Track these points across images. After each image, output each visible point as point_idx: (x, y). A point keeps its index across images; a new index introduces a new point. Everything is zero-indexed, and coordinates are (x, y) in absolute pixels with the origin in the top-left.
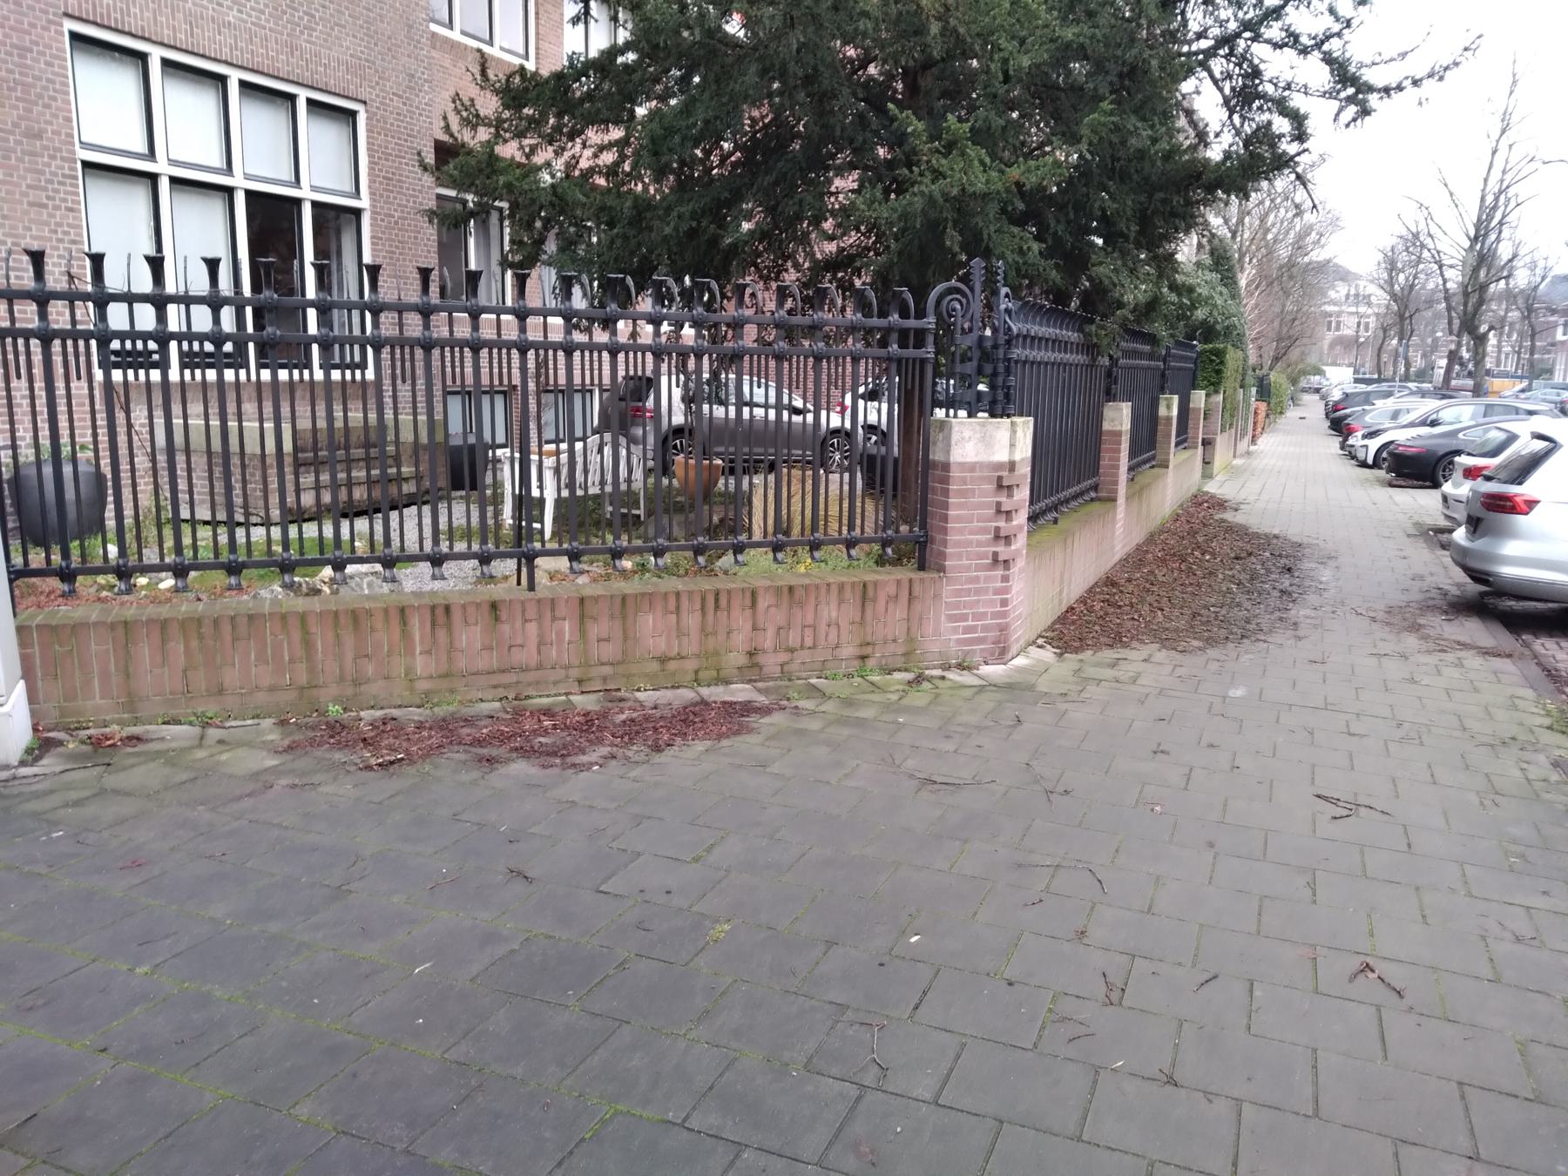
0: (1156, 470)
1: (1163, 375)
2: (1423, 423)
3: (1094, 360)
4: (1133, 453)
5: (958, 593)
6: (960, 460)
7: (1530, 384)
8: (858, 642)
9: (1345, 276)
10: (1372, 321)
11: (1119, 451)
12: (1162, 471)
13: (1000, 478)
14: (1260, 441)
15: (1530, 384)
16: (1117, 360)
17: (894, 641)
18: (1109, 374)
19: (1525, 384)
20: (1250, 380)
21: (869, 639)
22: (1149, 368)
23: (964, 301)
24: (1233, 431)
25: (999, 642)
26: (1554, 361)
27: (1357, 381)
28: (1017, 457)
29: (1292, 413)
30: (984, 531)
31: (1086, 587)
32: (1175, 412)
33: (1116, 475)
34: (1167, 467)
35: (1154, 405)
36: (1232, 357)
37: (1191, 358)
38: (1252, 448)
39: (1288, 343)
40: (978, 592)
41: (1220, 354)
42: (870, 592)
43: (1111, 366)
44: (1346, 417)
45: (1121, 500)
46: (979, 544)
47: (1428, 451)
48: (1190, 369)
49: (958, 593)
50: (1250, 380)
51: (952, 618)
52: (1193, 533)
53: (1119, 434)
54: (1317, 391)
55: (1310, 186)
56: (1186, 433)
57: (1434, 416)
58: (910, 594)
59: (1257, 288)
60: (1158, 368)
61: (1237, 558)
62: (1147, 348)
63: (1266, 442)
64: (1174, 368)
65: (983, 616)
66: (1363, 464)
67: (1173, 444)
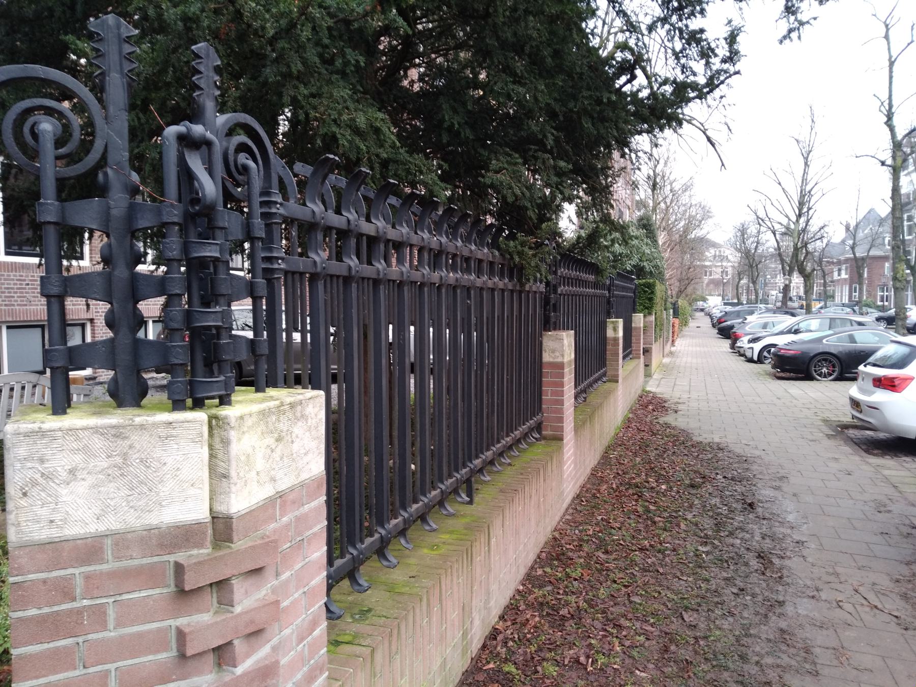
0: (608, 384)
1: (609, 302)
2: (789, 332)
3: (522, 285)
6: (43, 534)
7: (826, 304)
9: (714, 245)
10: (730, 270)
11: (562, 385)
14: (676, 343)
15: (826, 304)
18: (546, 301)
19: (822, 304)
20: (669, 305)
22: (595, 296)
24: (662, 339)
26: (834, 291)
27: (725, 304)
29: (692, 324)
31: (523, 571)
32: (621, 334)
33: (561, 411)
34: (617, 381)
35: (603, 327)
36: (659, 288)
37: (631, 289)
38: (673, 349)
39: (687, 282)
41: (651, 286)
44: (732, 327)
47: (803, 353)
48: (631, 297)
50: (669, 305)
52: (644, 447)
53: (561, 366)
54: (702, 310)
55: (717, 146)
56: (631, 347)
57: (796, 327)
59: (668, 247)
60: (603, 296)
61: (692, 486)
62: (591, 278)
63: (681, 344)
64: (617, 296)
66: (751, 360)
67: (621, 356)
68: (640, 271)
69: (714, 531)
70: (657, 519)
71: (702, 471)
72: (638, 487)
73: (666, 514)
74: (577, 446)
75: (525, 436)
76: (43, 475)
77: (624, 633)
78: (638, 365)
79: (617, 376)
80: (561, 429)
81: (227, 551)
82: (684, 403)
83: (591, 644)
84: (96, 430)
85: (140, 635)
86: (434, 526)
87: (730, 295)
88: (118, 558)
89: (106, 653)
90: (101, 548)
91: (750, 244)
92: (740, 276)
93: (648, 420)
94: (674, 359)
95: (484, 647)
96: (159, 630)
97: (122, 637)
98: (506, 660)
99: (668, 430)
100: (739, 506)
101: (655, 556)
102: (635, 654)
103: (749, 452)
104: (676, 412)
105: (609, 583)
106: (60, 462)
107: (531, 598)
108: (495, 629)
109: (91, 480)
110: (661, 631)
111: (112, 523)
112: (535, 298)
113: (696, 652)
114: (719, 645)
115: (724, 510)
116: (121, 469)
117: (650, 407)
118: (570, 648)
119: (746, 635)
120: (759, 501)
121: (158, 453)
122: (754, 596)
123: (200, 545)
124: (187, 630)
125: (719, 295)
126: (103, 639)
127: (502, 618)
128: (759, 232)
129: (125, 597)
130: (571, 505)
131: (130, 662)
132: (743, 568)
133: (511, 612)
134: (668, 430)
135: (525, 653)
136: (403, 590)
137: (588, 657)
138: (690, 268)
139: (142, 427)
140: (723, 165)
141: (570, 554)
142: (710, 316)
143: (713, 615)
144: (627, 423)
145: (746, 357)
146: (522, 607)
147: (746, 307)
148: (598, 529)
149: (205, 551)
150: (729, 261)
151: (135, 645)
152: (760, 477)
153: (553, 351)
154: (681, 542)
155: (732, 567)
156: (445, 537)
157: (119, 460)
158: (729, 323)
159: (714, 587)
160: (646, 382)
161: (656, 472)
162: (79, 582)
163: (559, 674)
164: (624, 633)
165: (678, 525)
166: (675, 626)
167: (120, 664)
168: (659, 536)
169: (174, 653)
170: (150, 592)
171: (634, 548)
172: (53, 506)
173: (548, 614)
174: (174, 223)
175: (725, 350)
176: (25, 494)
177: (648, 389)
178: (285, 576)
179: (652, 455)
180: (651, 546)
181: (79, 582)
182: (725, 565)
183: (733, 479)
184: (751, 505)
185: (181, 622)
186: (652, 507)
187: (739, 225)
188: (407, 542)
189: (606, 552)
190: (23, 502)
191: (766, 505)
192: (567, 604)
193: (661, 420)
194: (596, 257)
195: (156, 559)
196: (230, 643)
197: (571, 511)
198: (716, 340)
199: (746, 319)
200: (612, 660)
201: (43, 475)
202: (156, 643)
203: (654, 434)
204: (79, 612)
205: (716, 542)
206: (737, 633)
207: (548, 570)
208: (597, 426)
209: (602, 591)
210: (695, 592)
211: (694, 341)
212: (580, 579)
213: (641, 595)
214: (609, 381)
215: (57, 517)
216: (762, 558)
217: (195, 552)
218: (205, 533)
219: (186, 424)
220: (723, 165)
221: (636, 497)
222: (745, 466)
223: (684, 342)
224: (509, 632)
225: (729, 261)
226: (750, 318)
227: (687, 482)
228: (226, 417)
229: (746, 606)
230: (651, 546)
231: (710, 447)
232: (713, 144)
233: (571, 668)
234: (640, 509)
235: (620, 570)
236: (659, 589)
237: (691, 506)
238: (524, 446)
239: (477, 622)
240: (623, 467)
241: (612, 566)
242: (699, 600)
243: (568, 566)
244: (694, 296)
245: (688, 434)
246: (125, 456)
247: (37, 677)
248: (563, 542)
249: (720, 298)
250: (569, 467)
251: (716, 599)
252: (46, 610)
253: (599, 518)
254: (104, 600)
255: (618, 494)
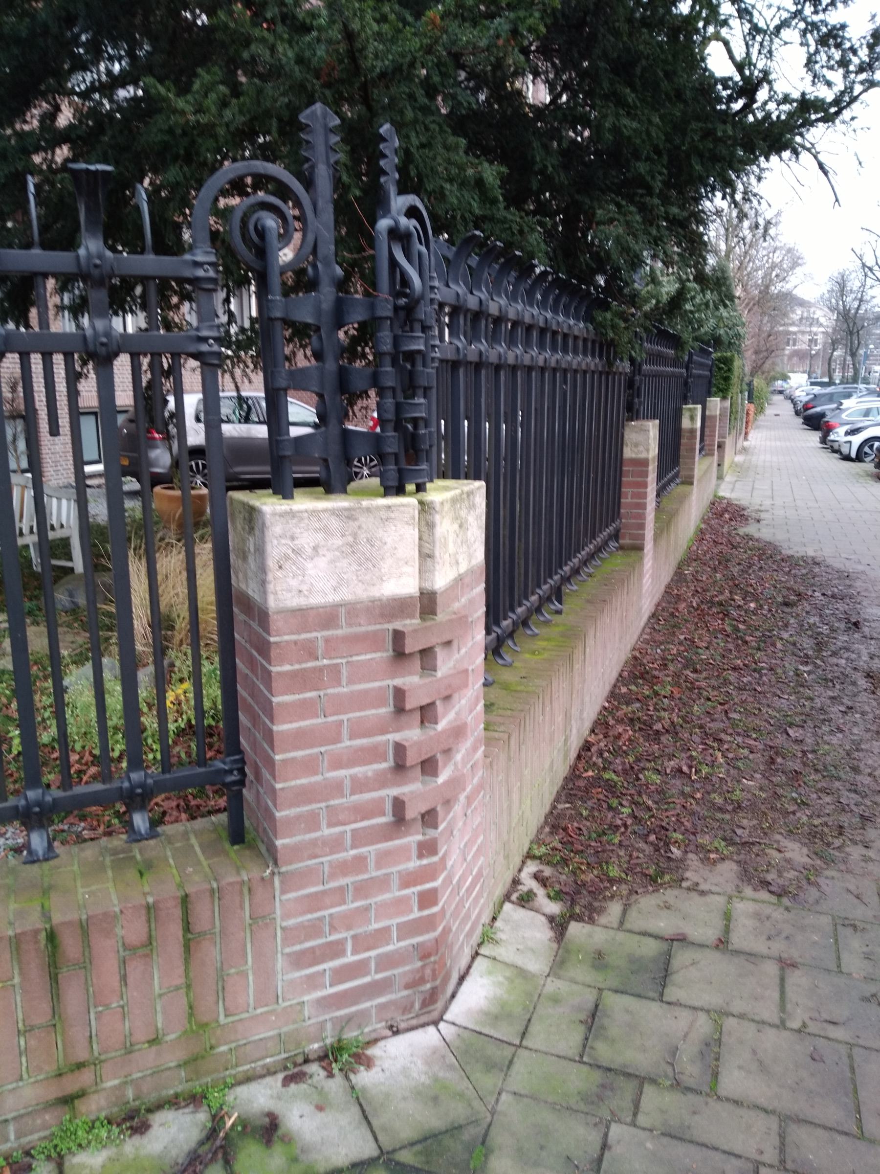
1: (686, 383)
3: (610, 364)
4: (661, 474)
5: (314, 902)
6: (293, 601)
8: (50, 1069)
9: (802, 303)
10: (820, 338)
11: (645, 485)
12: (682, 489)
13: (398, 637)
16: (640, 365)
17: (154, 1041)
18: (630, 384)
21: (82, 1055)
22: (673, 375)
23: (291, 211)
25: (422, 980)
27: (812, 384)
28: (441, 580)
29: (769, 411)
30: (373, 754)
31: (608, 688)
33: (642, 517)
34: (692, 484)
36: (737, 363)
37: (707, 365)
38: (746, 444)
39: (765, 354)
40: (361, 890)
42: (71, 946)
43: (633, 373)
44: (822, 415)
45: (649, 546)
46: (359, 786)
48: (706, 376)
49: (314, 902)
51: (299, 960)
52: (724, 561)
53: (644, 463)
54: (781, 392)
58: (187, 927)
61: (786, 604)
62: (671, 352)
63: (756, 438)
65: (383, 935)
66: (847, 458)
68: (717, 341)
69: (815, 651)
70: (748, 638)
71: (796, 587)
72: (722, 605)
73: (758, 634)
74: (655, 558)
75: (606, 543)
76: (293, 550)
77: (726, 746)
78: (711, 464)
79: (692, 477)
80: (642, 537)
81: (432, 622)
82: (767, 511)
83: (691, 756)
84: (333, 512)
85: (366, 692)
86: (536, 631)
87: (819, 372)
88: (350, 625)
89: (341, 705)
90: (337, 616)
91: (851, 301)
92: (834, 344)
93: (725, 530)
94: (748, 457)
95: (579, 757)
96: (380, 688)
97: (352, 692)
98: (604, 769)
99: (751, 543)
100: (842, 626)
101: (751, 675)
102: (740, 764)
103: (850, 567)
104: (758, 521)
105: (702, 700)
106: (306, 540)
107: (620, 714)
108: (587, 741)
109: (329, 556)
110: (765, 745)
111: (346, 595)
112: (620, 380)
113: (805, 764)
114: (828, 758)
115: (825, 629)
116: (352, 549)
117: (727, 516)
118: (670, 760)
119: (857, 750)
120: (865, 620)
121: (380, 533)
122: (863, 714)
123: (412, 616)
124: (405, 688)
125: (804, 372)
126: (338, 694)
127: (593, 731)
128: (863, 286)
129: (355, 658)
130: (647, 624)
131: (358, 714)
132: (850, 687)
133: (601, 725)
134: (751, 543)
135: (624, 763)
136: (519, 688)
137: (690, 767)
138: (769, 336)
139: (368, 510)
140: (837, 200)
141: (656, 673)
142: (792, 401)
143: (819, 732)
144: (700, 536)
145: (841, 454)
146: (612, 722)
147: (840, 389)
148: (682, 648)
149: (417, 621)
150: (821, 325)
151: (361, 701)
152: (866, 594)
153: (636, 445)
154: (778, 662)
155: (838, 686)
156: (543, 644)
157: (350, 539)
158: (818, 409)
159: (819, 705)
160: (718, 486)
161: (742, 589)
162: (321, 644)
163: (662, 782)
164: (726, 746)
165: (774, 645)
166: (780, 740)
167: (351, 715)
168: (753, 656)
169: (391, 708)
170: (374, 655)
171: (726, 667)
172: (300, 578)
173: (640, 729)
174: (387, 318)
175: (813, 444)
176: (280, 567)
177: (721, 494)
178: (463, 651)
179: (735, 570)
180: (744, 665)
181: (321, 644)
182: (830, 684)
183: (833, 596)
184: (856, 624)
185: (398, 682)
186: (741, 626)
187: (836, 274)
188: (515, 644)
189: (695, 671)
190: (279, 574)
191: (873, 625)
192: (660, 719)
193: (742, 531)
194: (677, 327)
195: (378, 627)
196: (433, 704)
197: (648, 630)
198: (801, 432)
199: (841, 404)
200: (717, 770)
201: (293, 550)
202: (377, 699)
203: (734, 547)
204: (321, 669)
205: (818, 662)
206: (848, 747)
207: (633, 688)
208: (672, 536)
209: (696, 708)
210: (799, 709)
211: (773, 433)
212: (671, 697)
213: (740, 712)
214: (683, 483)
215: (304, 588)
216: (872, 677)
217: (408, 622)
218: (415, 606)
219: (402, 509)
220: (837, 200)
221: (721, 615)
222: (847, 582)
223: (760, 435)
224: (602, 744)
225: (821, 325)
226: (846, 403)
227: (780, 599)
228: (432, 502)
229: (855, 723)
230: (744, 665)
231: (804, 561)
232: (826, 173)
233: (674, 777)
234: (729, 629)
235: (713, 688)
236: (758, 706)
237: (786, 625)
238: (604, 555)
239: (574, 731)
240: (701, 584)
241: (703, 684)
242: (804, 717)
243: (656, 684)
244: (772, 373)
245: (775, 547)
246: (355, 536)
247: (291, 722)
248: (645, 661)
249: (806, 376)
250: (647, 581)
251: (822, 717)
252: (297, 667)
253: (682, 637)
254: (339, 661)
255: (700, 613)
